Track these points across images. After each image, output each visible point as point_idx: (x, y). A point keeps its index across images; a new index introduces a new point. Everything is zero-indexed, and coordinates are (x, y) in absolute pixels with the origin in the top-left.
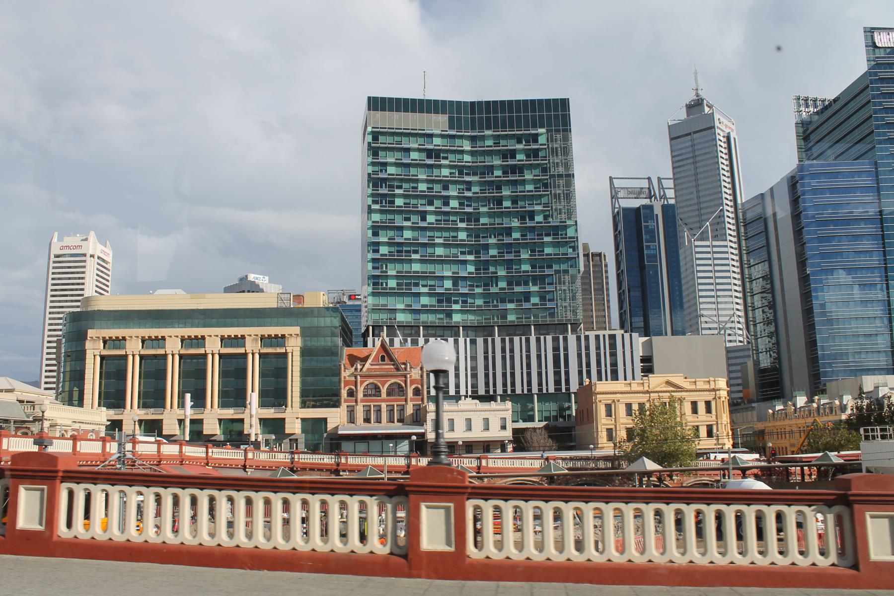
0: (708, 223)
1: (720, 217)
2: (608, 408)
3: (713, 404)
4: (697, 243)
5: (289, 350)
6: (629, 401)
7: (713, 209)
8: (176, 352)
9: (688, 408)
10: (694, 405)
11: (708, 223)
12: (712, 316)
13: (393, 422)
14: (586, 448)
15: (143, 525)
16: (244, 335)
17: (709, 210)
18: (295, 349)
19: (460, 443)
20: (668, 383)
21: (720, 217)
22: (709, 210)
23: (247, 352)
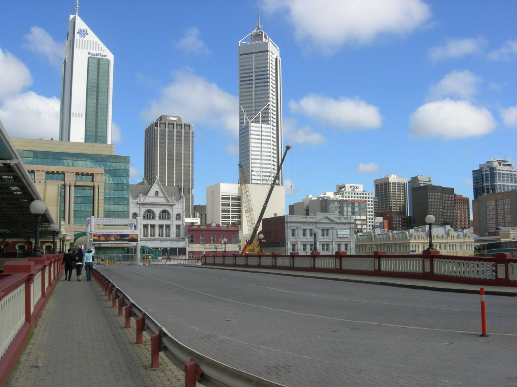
0: (260, 112)
1: (267, 109)
2: (293, 231)
4: (253, 124)
5: (96, 184)
6: (304, 228)
7: (263, 104)
8: (73, 183)
10: (304, 231)
11: (260, 112)
12: (258, 172)
13: (147, 236)
14: (500, 247)
15: (492, 268)
16: (64, 172)
17: (261, 104)
18: (100, 184)
19: (169, 249)
20: (327, 218)
21: (267, 109)
22: (261, 104)
23: (66, 184)
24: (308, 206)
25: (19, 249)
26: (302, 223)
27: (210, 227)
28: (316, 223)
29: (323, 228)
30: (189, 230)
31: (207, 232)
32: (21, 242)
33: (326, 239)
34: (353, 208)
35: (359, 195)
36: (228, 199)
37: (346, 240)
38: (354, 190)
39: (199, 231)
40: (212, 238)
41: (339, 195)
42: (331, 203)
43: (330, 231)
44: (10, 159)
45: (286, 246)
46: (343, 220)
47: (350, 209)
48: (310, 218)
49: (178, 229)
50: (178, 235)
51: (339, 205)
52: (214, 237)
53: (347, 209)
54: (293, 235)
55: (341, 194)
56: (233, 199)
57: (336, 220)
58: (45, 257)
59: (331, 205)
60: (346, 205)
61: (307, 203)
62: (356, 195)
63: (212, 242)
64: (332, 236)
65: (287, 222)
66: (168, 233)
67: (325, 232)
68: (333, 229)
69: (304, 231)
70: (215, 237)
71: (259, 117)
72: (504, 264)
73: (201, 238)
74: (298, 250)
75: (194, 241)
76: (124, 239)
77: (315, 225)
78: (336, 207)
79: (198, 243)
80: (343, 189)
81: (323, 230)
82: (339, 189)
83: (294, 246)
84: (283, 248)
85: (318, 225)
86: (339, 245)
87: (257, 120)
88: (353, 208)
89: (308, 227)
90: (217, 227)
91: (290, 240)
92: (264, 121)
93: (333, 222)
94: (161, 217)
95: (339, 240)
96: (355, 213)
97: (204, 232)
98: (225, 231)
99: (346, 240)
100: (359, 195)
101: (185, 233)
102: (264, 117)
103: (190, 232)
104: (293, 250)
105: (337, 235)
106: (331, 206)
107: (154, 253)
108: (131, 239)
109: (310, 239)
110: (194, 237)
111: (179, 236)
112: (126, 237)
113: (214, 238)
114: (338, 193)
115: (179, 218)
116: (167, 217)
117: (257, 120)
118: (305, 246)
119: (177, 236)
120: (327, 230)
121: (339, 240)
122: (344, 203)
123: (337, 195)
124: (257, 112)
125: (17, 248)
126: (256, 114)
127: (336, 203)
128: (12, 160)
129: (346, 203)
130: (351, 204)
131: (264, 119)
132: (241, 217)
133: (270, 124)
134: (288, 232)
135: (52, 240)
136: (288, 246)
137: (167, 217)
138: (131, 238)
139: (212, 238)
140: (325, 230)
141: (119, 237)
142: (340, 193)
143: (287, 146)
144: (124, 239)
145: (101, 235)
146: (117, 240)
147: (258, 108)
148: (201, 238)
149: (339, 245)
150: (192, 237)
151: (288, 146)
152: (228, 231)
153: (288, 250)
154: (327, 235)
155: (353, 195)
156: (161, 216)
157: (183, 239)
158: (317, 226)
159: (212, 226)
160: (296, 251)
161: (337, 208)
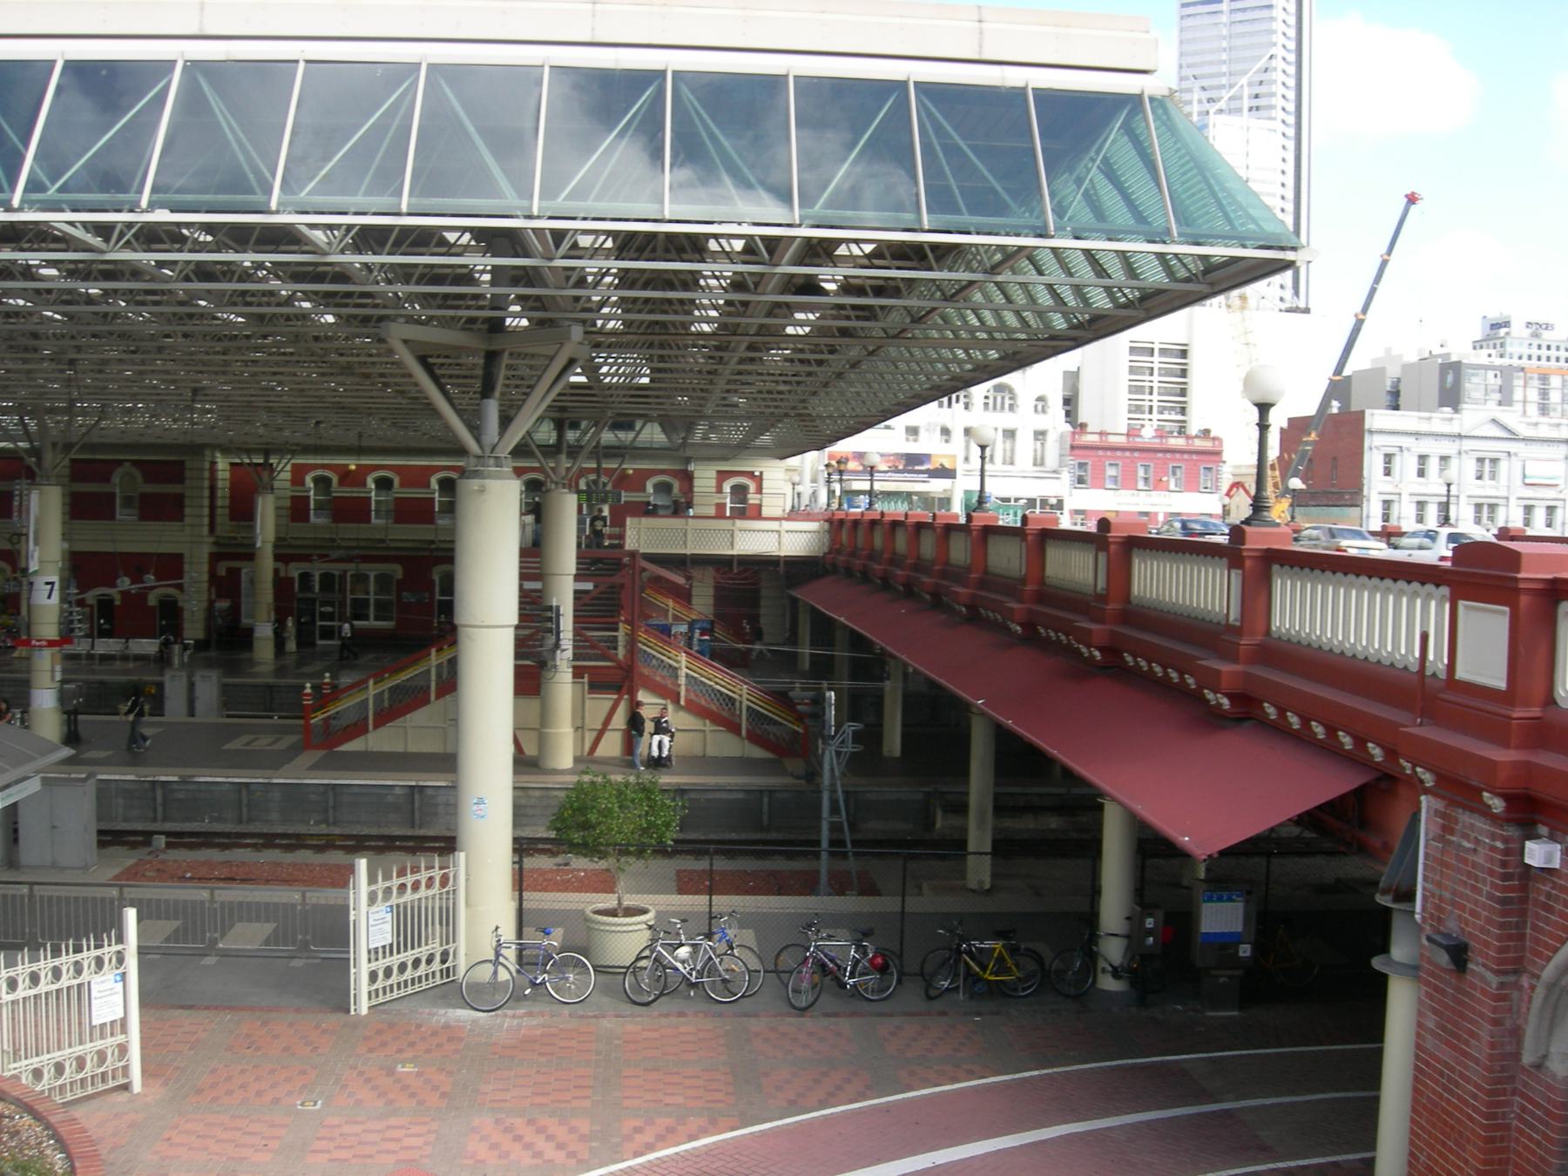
2: (1388, 458)
3: (1397, 462)
6: (1424, 451)
9: (1413, 465)
10: (1423, 459)
24: (1399, 380)
25: (315, 485)
26: (1417, 435)
27: (1138, 440)
28: (1460, 436)
29: (1481, 455)
30: (1073, 448)
31: (1128, 454)
32: (533, 469)
33: (1487, 489)
34: (1544, 394)
35: (1553, 353)
36: (1151, 352)
37: (1551, 493)
38: (1536, 335)
39: (1105, 449)
40: (1141, 473)
41: (1488, 347)
42: (1473, 375)
43: (1503, 466)
44: (1294, 249)
45: (1365, 505)
46: (1544, 431)
47: (1533, 395)
48: (1551, 425)
49: (1039, 443)
50: (1039, 461)
51: (1499, 381)
52: (1146, 468)
53: (1525, 396)
54: (1388, 472)
55: (1495, 347)
56: (1163, 352)
57: (1524, 431)
58: (118, 516)
59: (1475, 380)
60: (1521, 382)
61: (1393, 372)
62: (1544, 352)
63: (1141, 485)
64: (1509, 481)
65: (1371, 432)
66: (1008, 454)
67: (1487, 466)
68: (1513, 458)
69: (1423, 459)
70: (1151, 470)
71: (1241, 98)
72: (1507, 609)
73: (1111, 472)
74: (1399, 518)
75: (1088, 479)
76: (917, 468)
77: (1458, 441)
78: (1490, 388)
79: (1099, 483)
80: (1502, 331)
81: (1481, 460)
82: (1489, 332)
83: (1387, 504)
84: (1354, 511)
85: (1467, 445)
86: (1528, 509)
87: (1234, 105)
88: (1544, 394)
89: (1434, 448)
90: (1158, 441)
91: (1375, 484)
92: (1258, 108)
93: (1513, 437)
94: (991, 406)
95: (1529, 492)
96: (1548, 409)
97: (1119, 454)
98: (1182, 452)
99: (1551, 493)
100: (1553, 353)
101: (1061, 456)
102: (1257, 96)
103: (1077, 452)
104: (1386, 518)
105: (1524, 477)
106: (1473, 386)
107: (1011, 512)
108: (936, 470)
109: (1433, 485)
110: (1089, 467)
111: (1042, 464)
112: (921, 463)
113: (1146, 472)
114: (1484, 344)
115: (1043, 407)
116: (1007, 406)
117: (1234, 105)
118: (1421, 505)
119: (1035, 465)
120: (1494, 461)
121: (1529, 492)
122: (1515, 374)
123: (1481, 347)
124: (1233, 80)
125: (434, 485)
126: (1231, 86)
127: (1491, 374)
128: (1300, 252)
129: (1521, 374)
130: (1539, 379)
131: (1256, 102)
132: (1187, 411)
133: (1275, 119)
134: (1373, 464)
135: (594, 466)
136: (1368, 506)
137: (1007, 406)
138: (938, 465)
139: (1141, 473)
140: (1487, 461)
141: (903, 462)
142: (1491, 343)
143: (1409, 192)
144: (917, 468)
145: (850, 456)
146: (897, 471)
147: (1239, 67)
148: (1111, 472)
149: (1528, 509)
150: (1082, 466)
151: (1413, 194)
152: (1190, 452)
153: (1368, 517)
154: (1493, 476)
155: (1535, 352)
156: (991, 401)
157: (1054, 472)
158: (1464, 448)
159: (1140, 436)
160: (1393, 522)
161: (1493, 391)
